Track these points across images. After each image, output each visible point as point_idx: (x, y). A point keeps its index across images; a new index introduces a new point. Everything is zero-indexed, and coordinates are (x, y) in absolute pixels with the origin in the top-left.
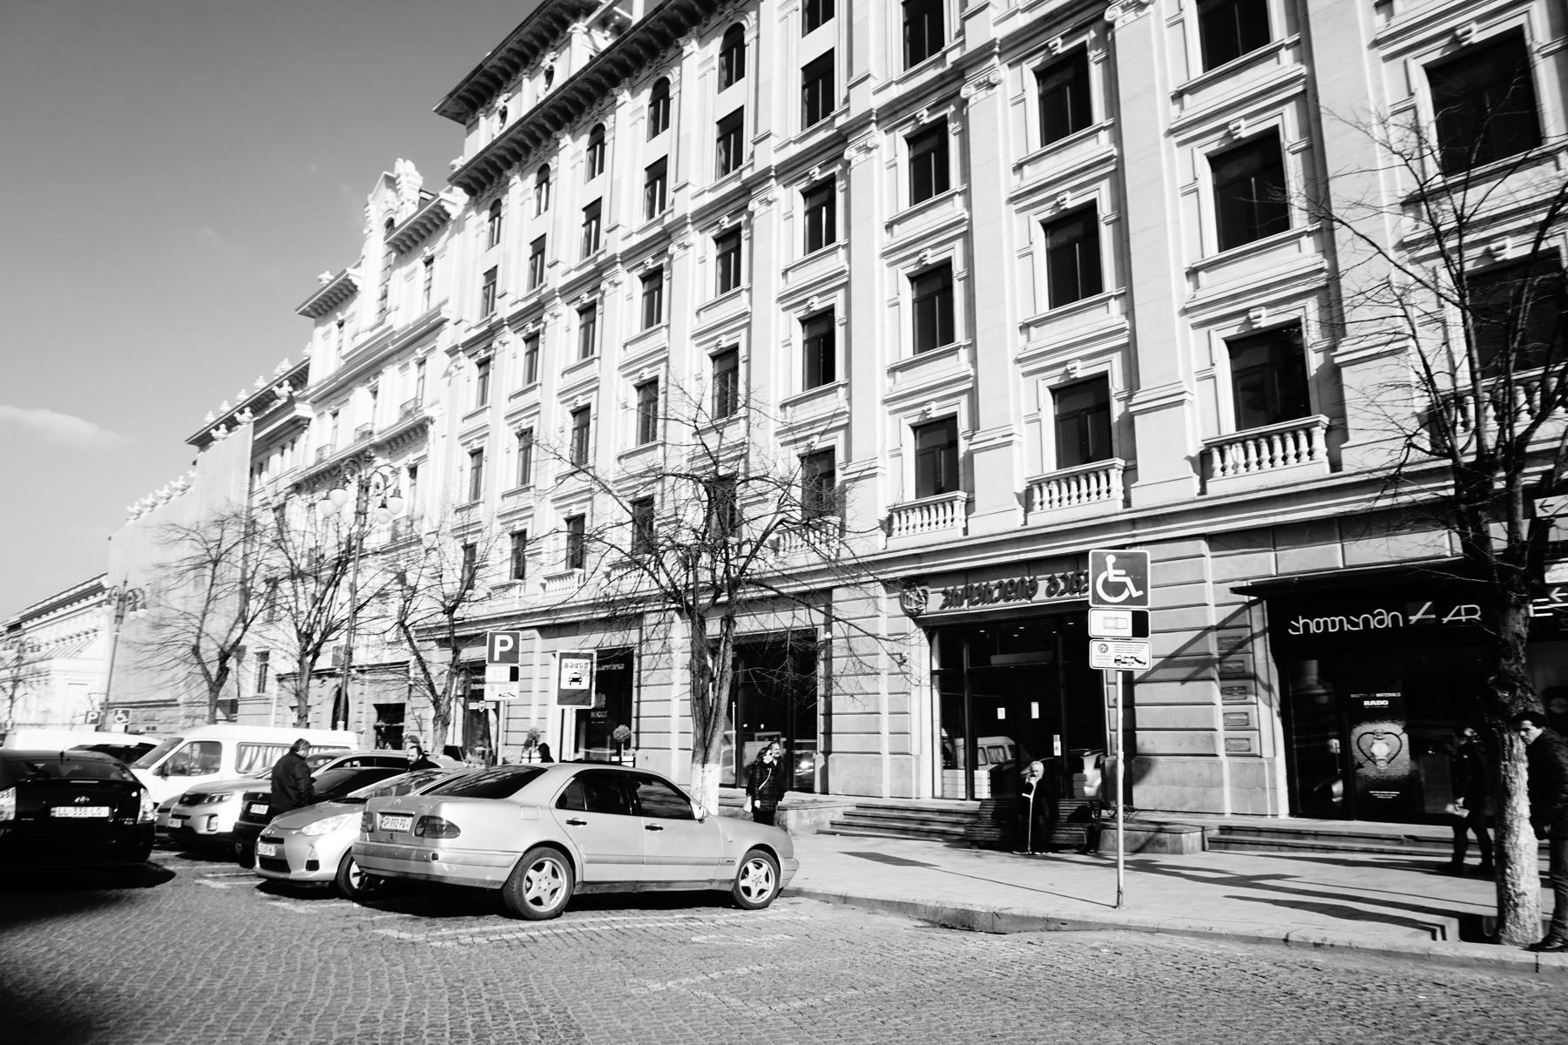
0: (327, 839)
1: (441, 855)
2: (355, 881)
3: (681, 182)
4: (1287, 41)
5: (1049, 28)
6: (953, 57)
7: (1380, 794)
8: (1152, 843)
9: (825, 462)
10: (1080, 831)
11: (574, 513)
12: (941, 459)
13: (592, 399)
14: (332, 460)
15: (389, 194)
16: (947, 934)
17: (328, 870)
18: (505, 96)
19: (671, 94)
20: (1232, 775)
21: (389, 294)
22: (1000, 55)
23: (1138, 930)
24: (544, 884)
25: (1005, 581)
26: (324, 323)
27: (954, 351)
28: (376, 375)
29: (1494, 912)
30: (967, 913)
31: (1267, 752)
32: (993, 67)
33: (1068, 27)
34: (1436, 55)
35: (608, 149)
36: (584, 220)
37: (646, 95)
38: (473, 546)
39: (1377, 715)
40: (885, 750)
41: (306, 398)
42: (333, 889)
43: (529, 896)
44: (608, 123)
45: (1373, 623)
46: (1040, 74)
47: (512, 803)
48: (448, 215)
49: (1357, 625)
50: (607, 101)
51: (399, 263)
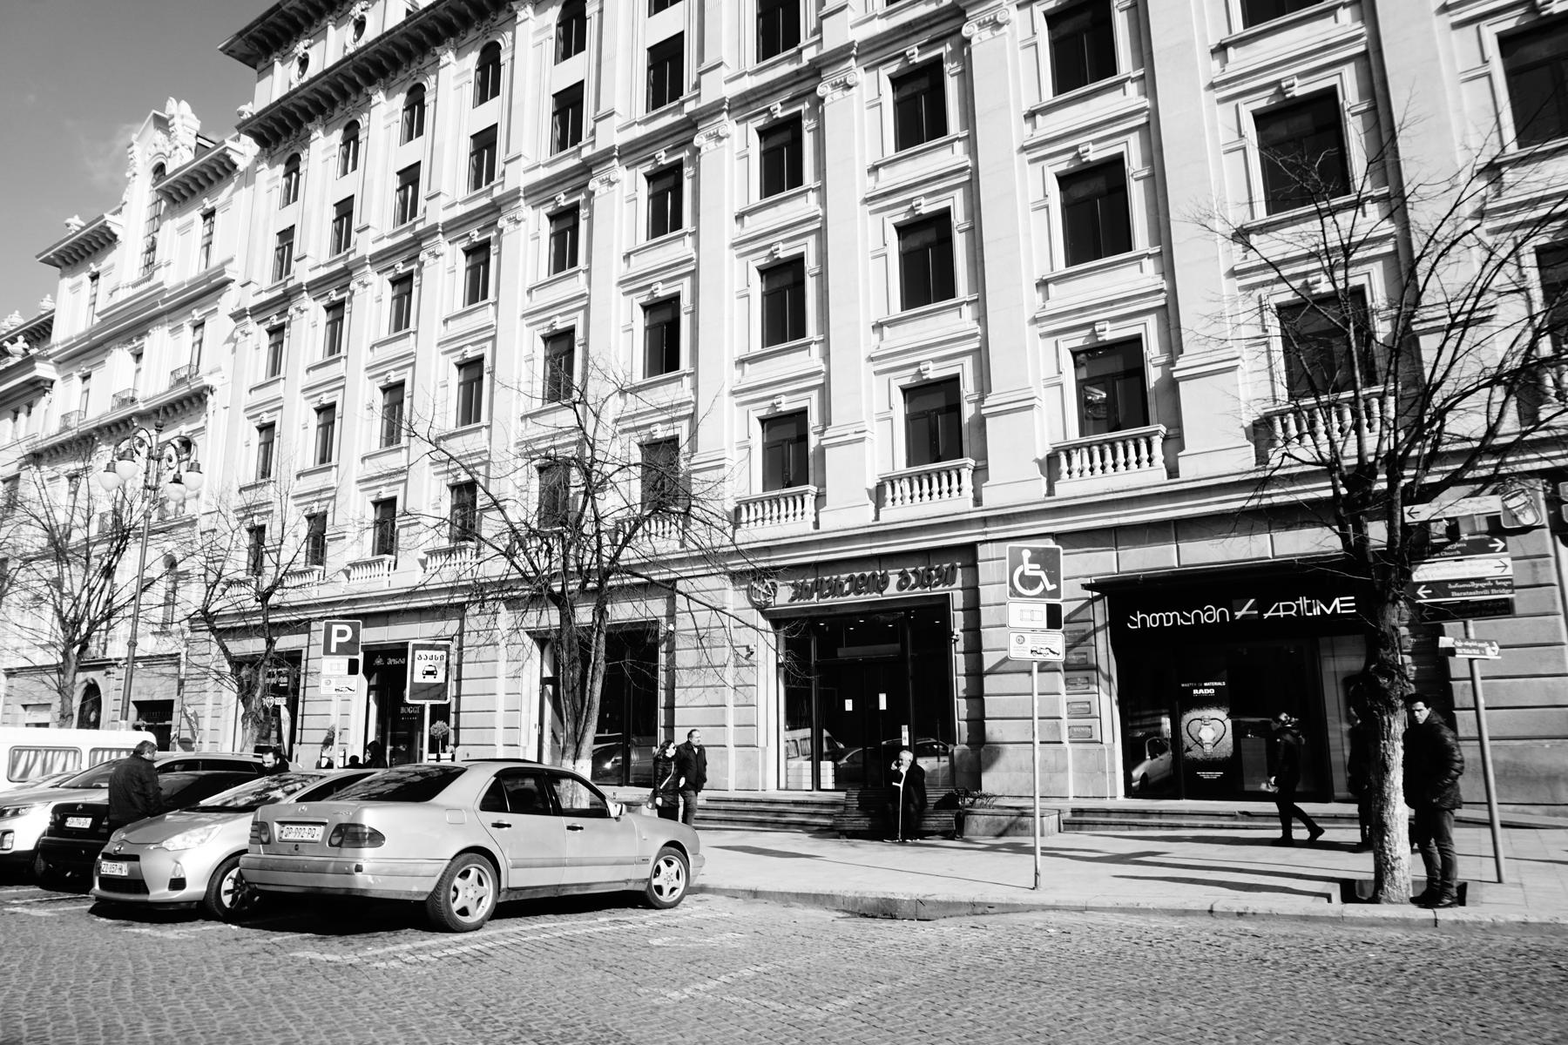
0: (192, 852)
1: (365, 866)
2: (227, 900)
3: (433, 191)
4: (1133, 75)
5: (907, 37)
6: (809, 54)
7: (1206, 775)
8: (1013, 828)
9: (794, 426)
10: (947, 817)
11: (384, 496)
12: (790, 450)
13: (277, 417)
14: (83, 429)
15: (159, 136)
16: (866, 922)
17: (196, 888)
18: (307, 42)
19: (502, 60)
20: (1074, 760)
21: (155, 248)
22: (857, 58)
23: (1067, 909)
24: (470, 893)
25: (857, 575)
26: (73, 274)
27: (807, 346)
28: (140, 337)
29: (1372, 877)
30: (889, 901)
31: (1107, 739)
32: (849, 69)
33: (924, 38)
34: (1263, 103)
35: (362, 147)
36: (334, 216)
37: (473, 59)
38: (262, 529)
39: (1205, 703)
40: (730, 743)
41: (49, 357)
42: (202, 910)
43: (456, 907)
44: (363, 121)
45: (1204, 618)
46: (896, 81)
47: (436, 806)
48: (234, 166)
49: (1188, 620)
50: (428, 60)
51: (171, 213)
